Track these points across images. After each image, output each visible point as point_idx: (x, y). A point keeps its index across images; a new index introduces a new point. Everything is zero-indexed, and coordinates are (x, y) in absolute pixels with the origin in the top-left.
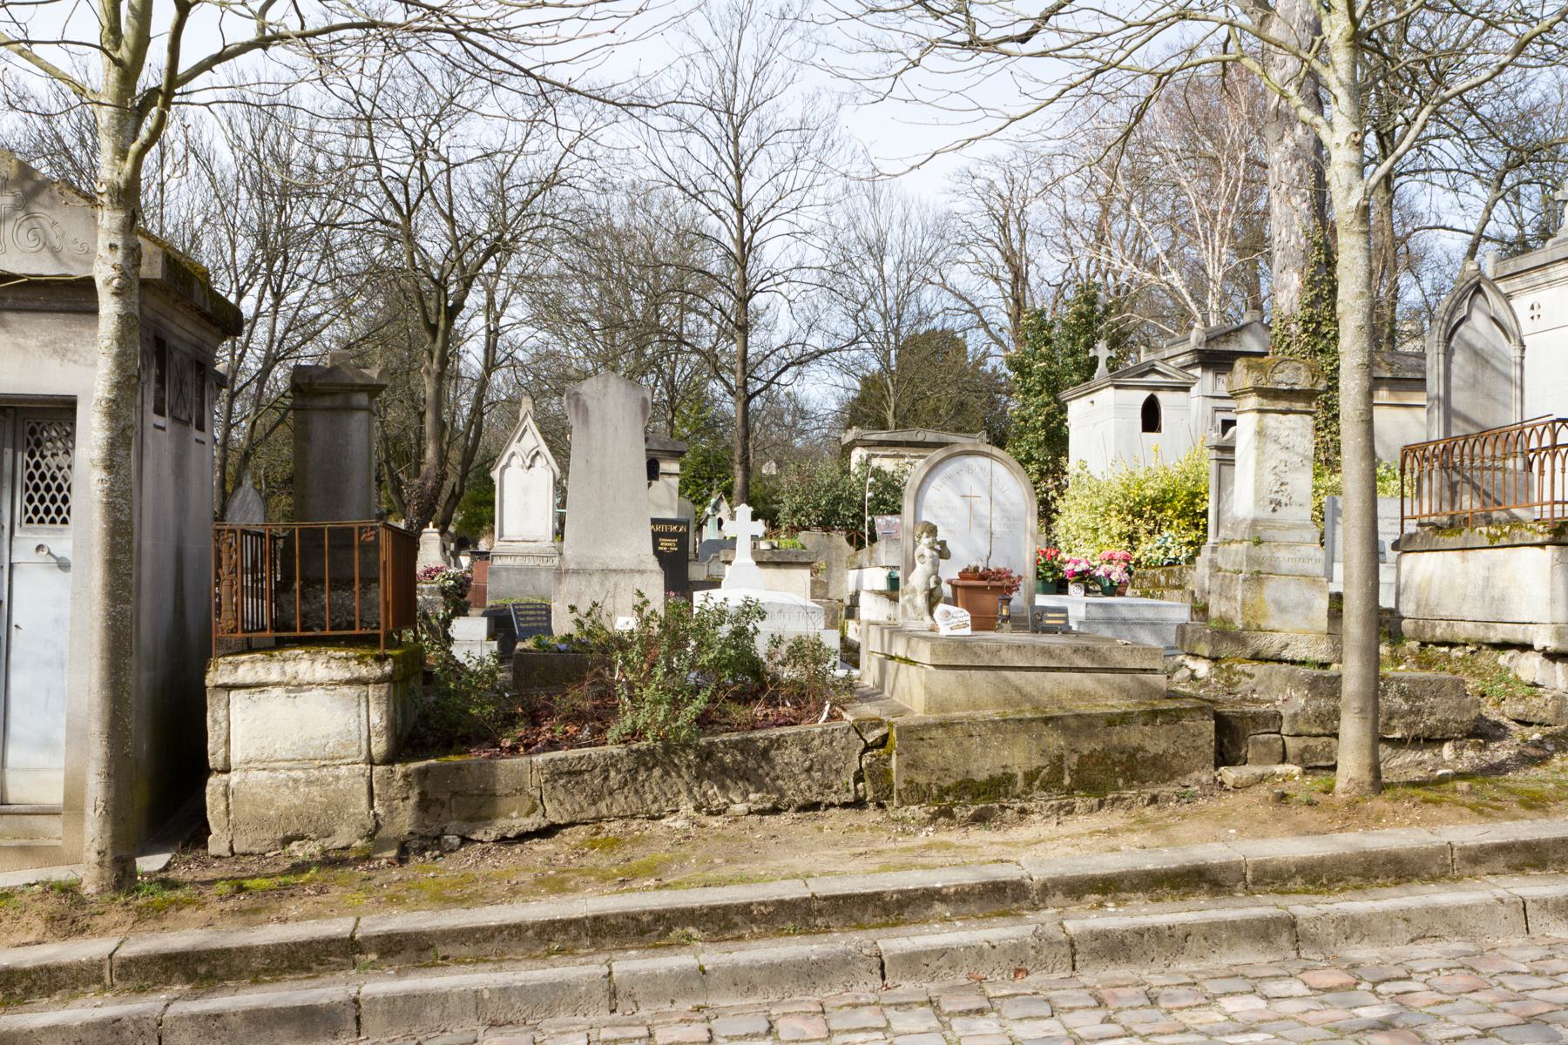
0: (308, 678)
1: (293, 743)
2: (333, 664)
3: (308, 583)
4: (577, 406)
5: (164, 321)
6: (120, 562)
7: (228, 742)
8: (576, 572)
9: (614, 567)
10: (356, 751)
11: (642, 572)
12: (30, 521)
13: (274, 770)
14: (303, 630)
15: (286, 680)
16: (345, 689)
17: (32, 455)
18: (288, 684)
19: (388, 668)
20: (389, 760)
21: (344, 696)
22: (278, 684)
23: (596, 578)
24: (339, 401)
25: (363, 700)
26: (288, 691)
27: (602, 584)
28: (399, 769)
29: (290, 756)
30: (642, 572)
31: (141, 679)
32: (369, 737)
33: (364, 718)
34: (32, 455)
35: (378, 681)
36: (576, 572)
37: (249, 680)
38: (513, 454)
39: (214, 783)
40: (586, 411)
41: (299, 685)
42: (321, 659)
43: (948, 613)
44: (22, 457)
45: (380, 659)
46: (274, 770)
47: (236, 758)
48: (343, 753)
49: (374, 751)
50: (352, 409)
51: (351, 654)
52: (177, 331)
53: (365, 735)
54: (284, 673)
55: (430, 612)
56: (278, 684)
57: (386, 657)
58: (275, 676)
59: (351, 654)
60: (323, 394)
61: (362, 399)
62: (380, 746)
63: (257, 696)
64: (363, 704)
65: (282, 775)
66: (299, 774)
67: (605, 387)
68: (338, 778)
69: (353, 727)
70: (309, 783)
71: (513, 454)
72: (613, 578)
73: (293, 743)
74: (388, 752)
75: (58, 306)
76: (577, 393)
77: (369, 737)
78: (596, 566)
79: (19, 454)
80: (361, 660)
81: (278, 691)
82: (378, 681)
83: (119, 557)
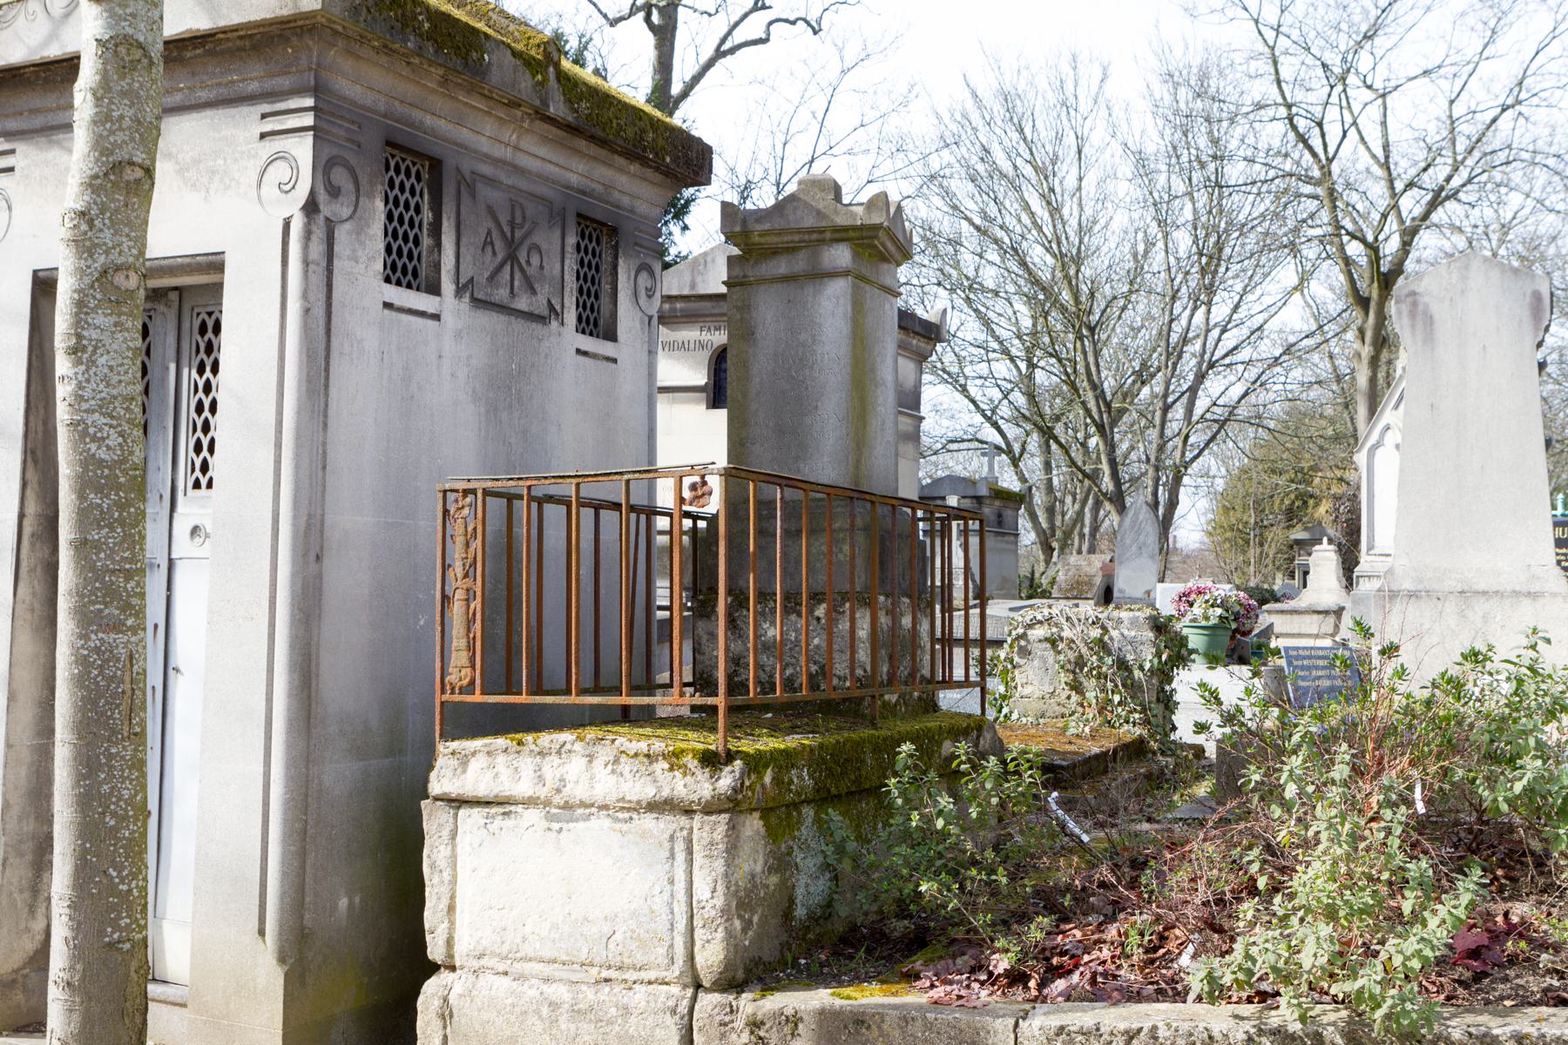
0: (578, 792)
1: (555, 927)
2: (626, 766)
3: (738, 599)
4: (1413, 315)
5: (417, 115)
6: (97, 546)
7: (451, 909)
8: (1413, 595)
9: (1482, 586)
10: (663, 959)
11: (1533, 596)
12: (197, 485)
13: (520, 978)
14: (531, 693)
15: (543, 793)
16: (648, 821)
17: (201, 371)
18: (547, 803)
19: (727, 780)
20: (732, 982)
21: (644, 835)
22: (530, 802)
23: (1450, 607)
24: (800, 263)
25: (680, 846)
26: (550, 818)
27: (1462, 614)
28: (747, 1004)
29: (548, 953)
30: (1533, 596)
31: (340, 773)
32: (691, 930)
33: (680, 887)
34: (201, 371)
35: (709, 809)
36: (1413, 595)
37: (483, 790)
38: (1388, 428)
39: (431, 988)
40: (1429, 321)
41: (567, 806)
42: (605, 753)
43: (195, 531)
44: (190, 375)
45: (711, 761)
46: (520, 978)
47: (460, 950)
48: (640, 958)
49: (699, 960)
50: (821, 275)
51: (658, 746)
52: (484, 145)
53: (681, 925)
54: (541, 779)
55: (1130, 657)
56: (530, 802)
57: (730, 757)
58: (524, 787)
59: (658, 746)
60: (775, 252)
61: (841, 256)
62: (711, 955)
63: (498, 821)
64: (681, 856)
65: (531, 991)
66: (560, 992)
67: (1464, 278)
68: (626, 1011)
69: (659, 903)
70: (577, 1013)
71: (1388, 428)
72: (1481, 606)
73: (555, 927)
74: (728, 965)
75: (203, 95)
76: (1413, 294)
77: (691, 930)
78: (1452, 584)
79: (185, 371)
80: (674, 759)
81: (533, 816)
82: (709, 809)
83: (95, 535)
